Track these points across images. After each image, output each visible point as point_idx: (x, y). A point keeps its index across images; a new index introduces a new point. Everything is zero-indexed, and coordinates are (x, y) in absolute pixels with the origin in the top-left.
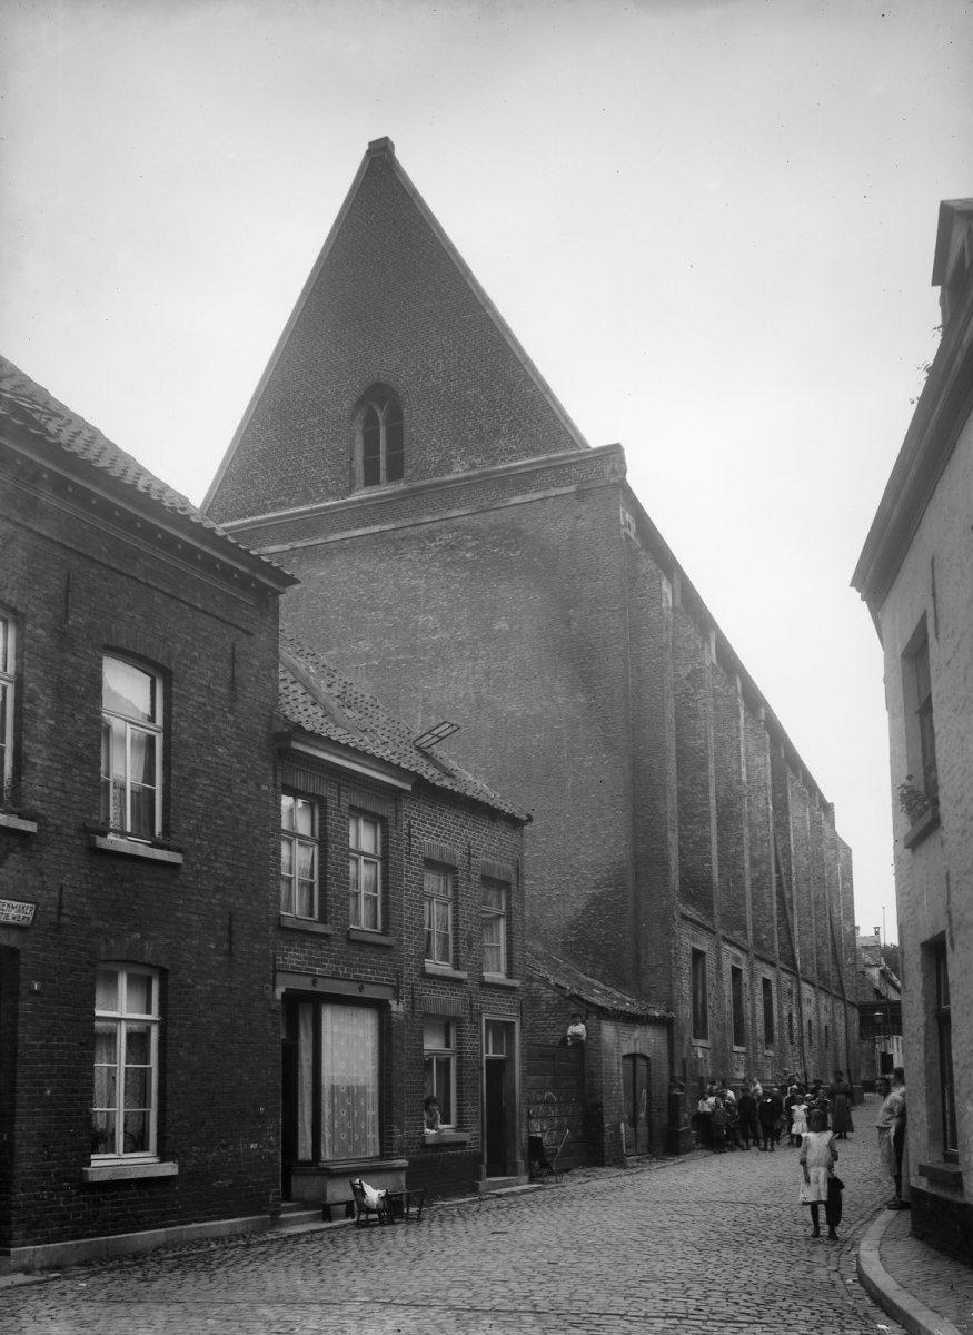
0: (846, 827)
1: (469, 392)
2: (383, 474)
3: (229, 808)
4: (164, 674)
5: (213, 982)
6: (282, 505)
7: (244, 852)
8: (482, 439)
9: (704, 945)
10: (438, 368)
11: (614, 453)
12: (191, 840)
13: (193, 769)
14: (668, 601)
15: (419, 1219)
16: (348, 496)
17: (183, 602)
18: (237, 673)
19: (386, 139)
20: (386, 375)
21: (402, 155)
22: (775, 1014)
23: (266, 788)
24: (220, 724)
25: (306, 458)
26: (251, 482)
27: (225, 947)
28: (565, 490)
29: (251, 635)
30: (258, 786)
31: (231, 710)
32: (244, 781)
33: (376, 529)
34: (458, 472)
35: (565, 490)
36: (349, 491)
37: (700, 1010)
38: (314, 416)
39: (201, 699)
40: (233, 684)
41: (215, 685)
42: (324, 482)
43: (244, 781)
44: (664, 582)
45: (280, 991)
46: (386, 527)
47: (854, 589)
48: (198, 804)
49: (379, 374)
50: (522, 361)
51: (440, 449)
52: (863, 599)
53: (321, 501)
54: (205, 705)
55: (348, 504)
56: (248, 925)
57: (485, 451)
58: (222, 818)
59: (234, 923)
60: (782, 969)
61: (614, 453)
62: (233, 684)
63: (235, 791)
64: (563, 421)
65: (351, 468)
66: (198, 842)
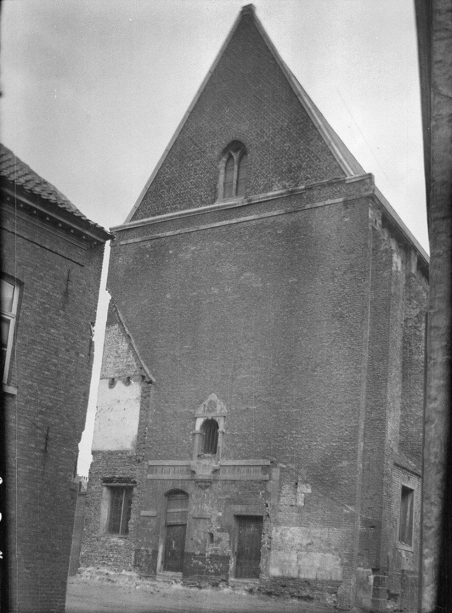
1: (285, 145)
2: (221, 192)
3: (55, 365)
4: (20, 285)
5: (31, 467)
6: (176, 209)
7: (62, 392)
10: (269, 131)
12: (26, 381)
13: (32, 340)
14: (397, 267)
16: (213, 204)
17: (36, 243)
18: (70, 287)
21: (260, 14)
23: (83, 356)
24: (55, 316)
27: (42, 447)
28: (337, 200)
29: (83, 266)
30: (77, 354)
31: (63, 308)
32: (67, 350)
34: (275, 190)
35: (337, 200)
36: (213, 201)
39: (42, 300)
40: (66, 293)
41: (53, 293)
43: (67, 350)
45: (199, 422)
48: (33, 361)
50: (297, 94)
53: (198, 207)
54: (45, 303)
55: (214, 208)
56: (60, 436)
57: (291, 178)
58: (49, 370)
59: (50, 434)
62: (66, 293)
63: (60, 355)
65: (215, 188)
66: (30, 383)
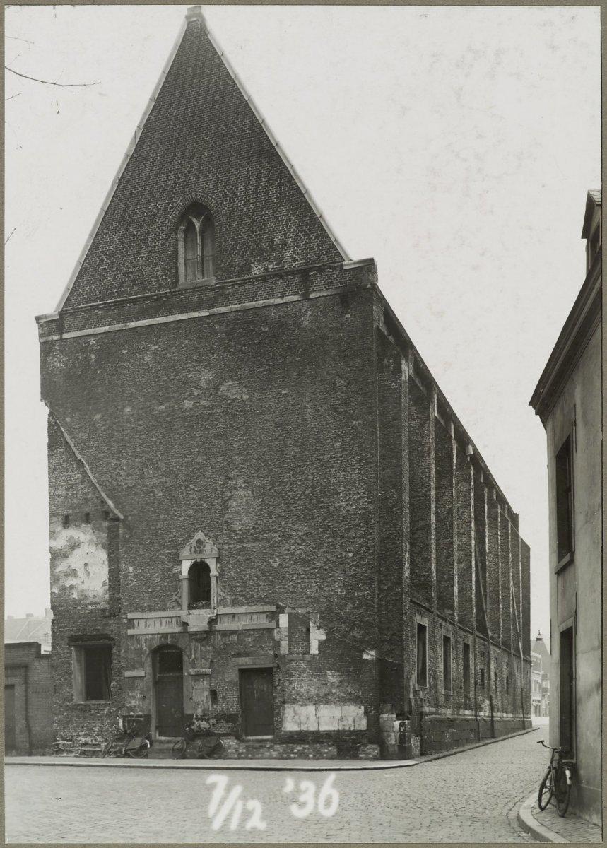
0: (525, 532)
8: (274, 250)
9: (425, 622)
11: (368, 266)
14: (406, 377)
15: (282, 720)
19: (371, 262)
20: (202, 196)
22: (472, 668)
25: (142, 258)
26: (100, 274)
33: (195, 314)
37: (577, 312)
38: (148, 225)
42: (157, 277)
44: (403, 362)
46: (203, 314)
47: (531, 407)
49: (196, 195)
51: (242, 256)
52: (536, 414)
60: (478, 637)
61: (368, 266)
64: (333, 240)
